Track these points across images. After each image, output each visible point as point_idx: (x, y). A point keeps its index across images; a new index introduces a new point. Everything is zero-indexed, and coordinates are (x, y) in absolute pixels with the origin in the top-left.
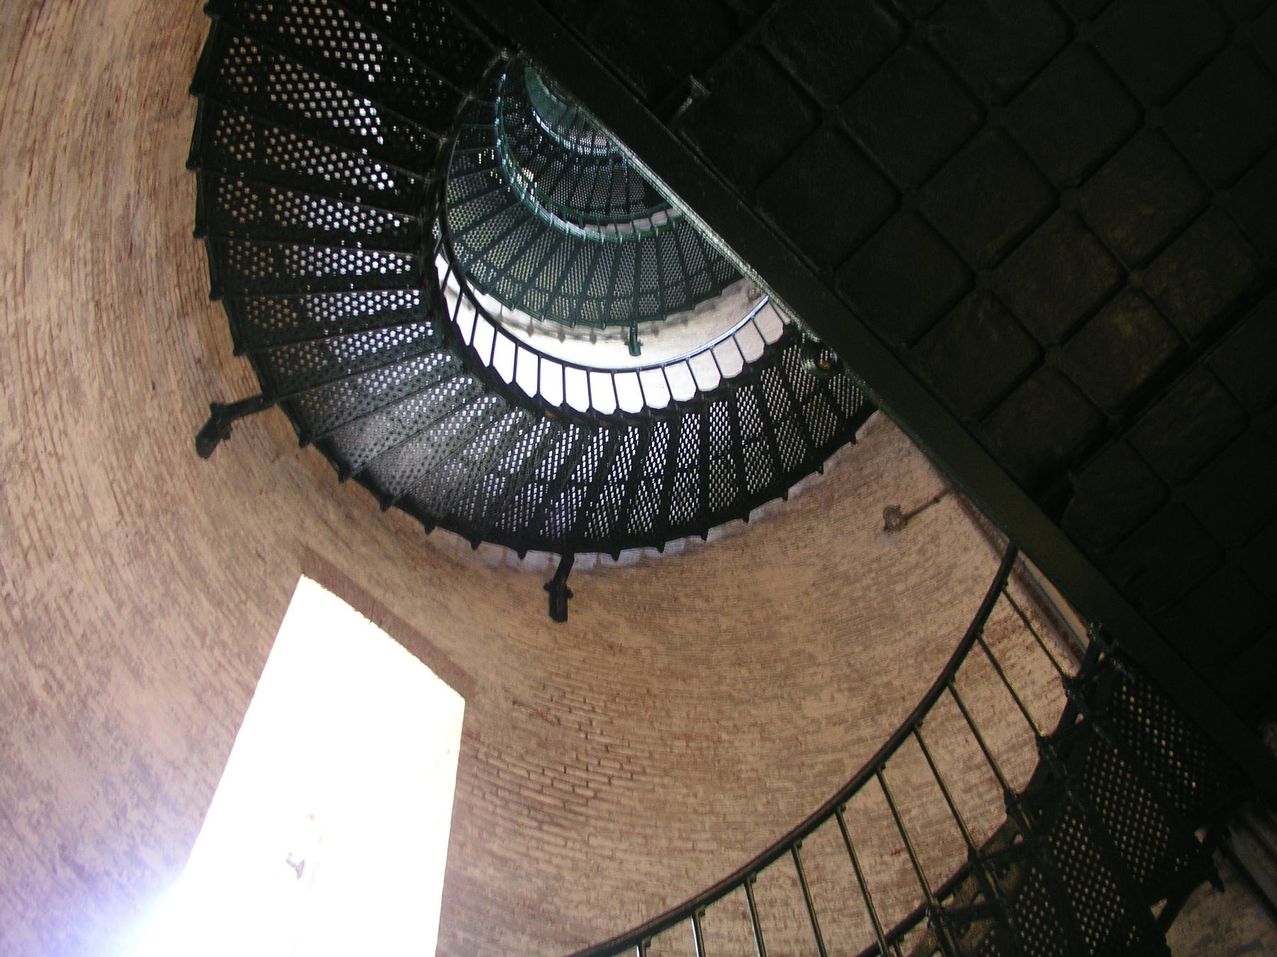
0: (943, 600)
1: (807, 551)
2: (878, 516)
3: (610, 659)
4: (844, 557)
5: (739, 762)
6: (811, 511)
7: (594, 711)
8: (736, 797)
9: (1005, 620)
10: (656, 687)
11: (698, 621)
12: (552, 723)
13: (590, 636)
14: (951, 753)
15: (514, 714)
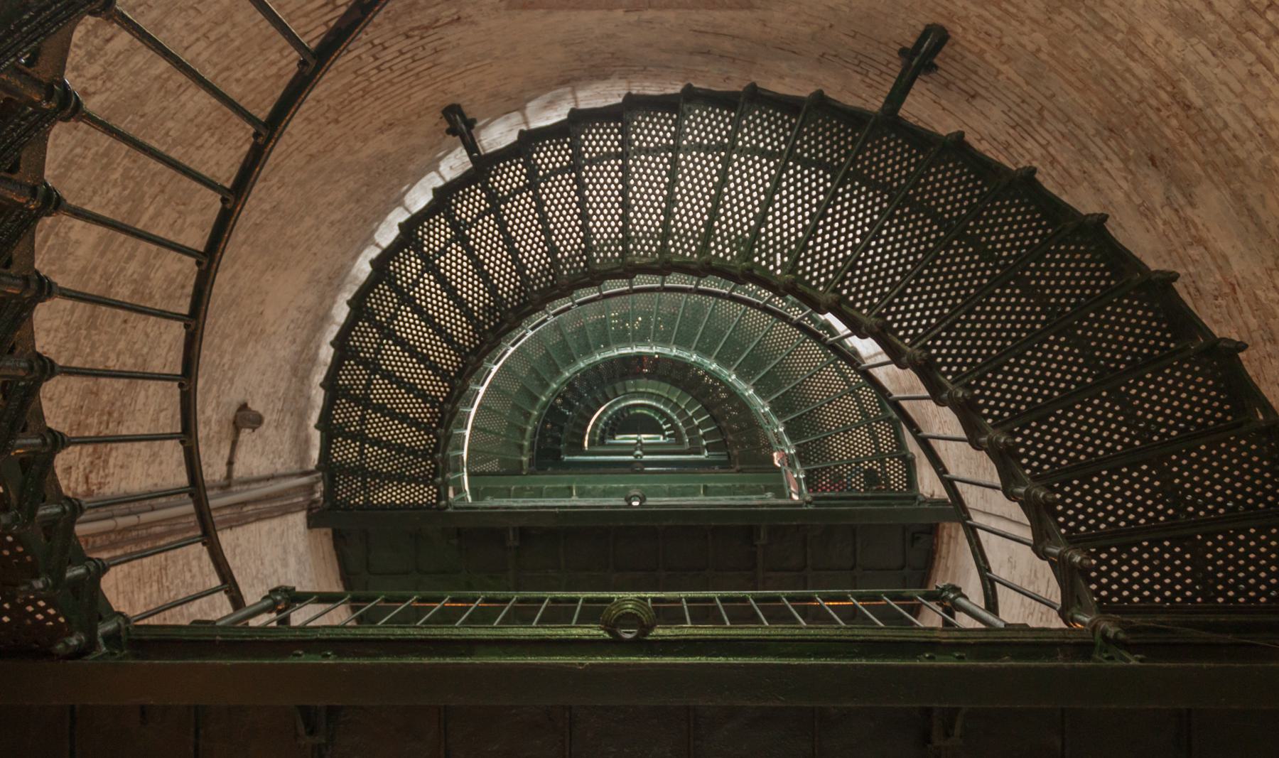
0: (162, 415)
1: (284, 327)
2: (257, 406)
3: (386, 117)
4: (256, 354)
5: (219, 141)
6: (302, 351)
7: (378, 68)
8: (200, 112)
9: (106, 462)
10: (334, 130)
11: (330, 204)
12: (412, 29)
13: (414, 118)
14: (48, 331)
15: (454, 10)
